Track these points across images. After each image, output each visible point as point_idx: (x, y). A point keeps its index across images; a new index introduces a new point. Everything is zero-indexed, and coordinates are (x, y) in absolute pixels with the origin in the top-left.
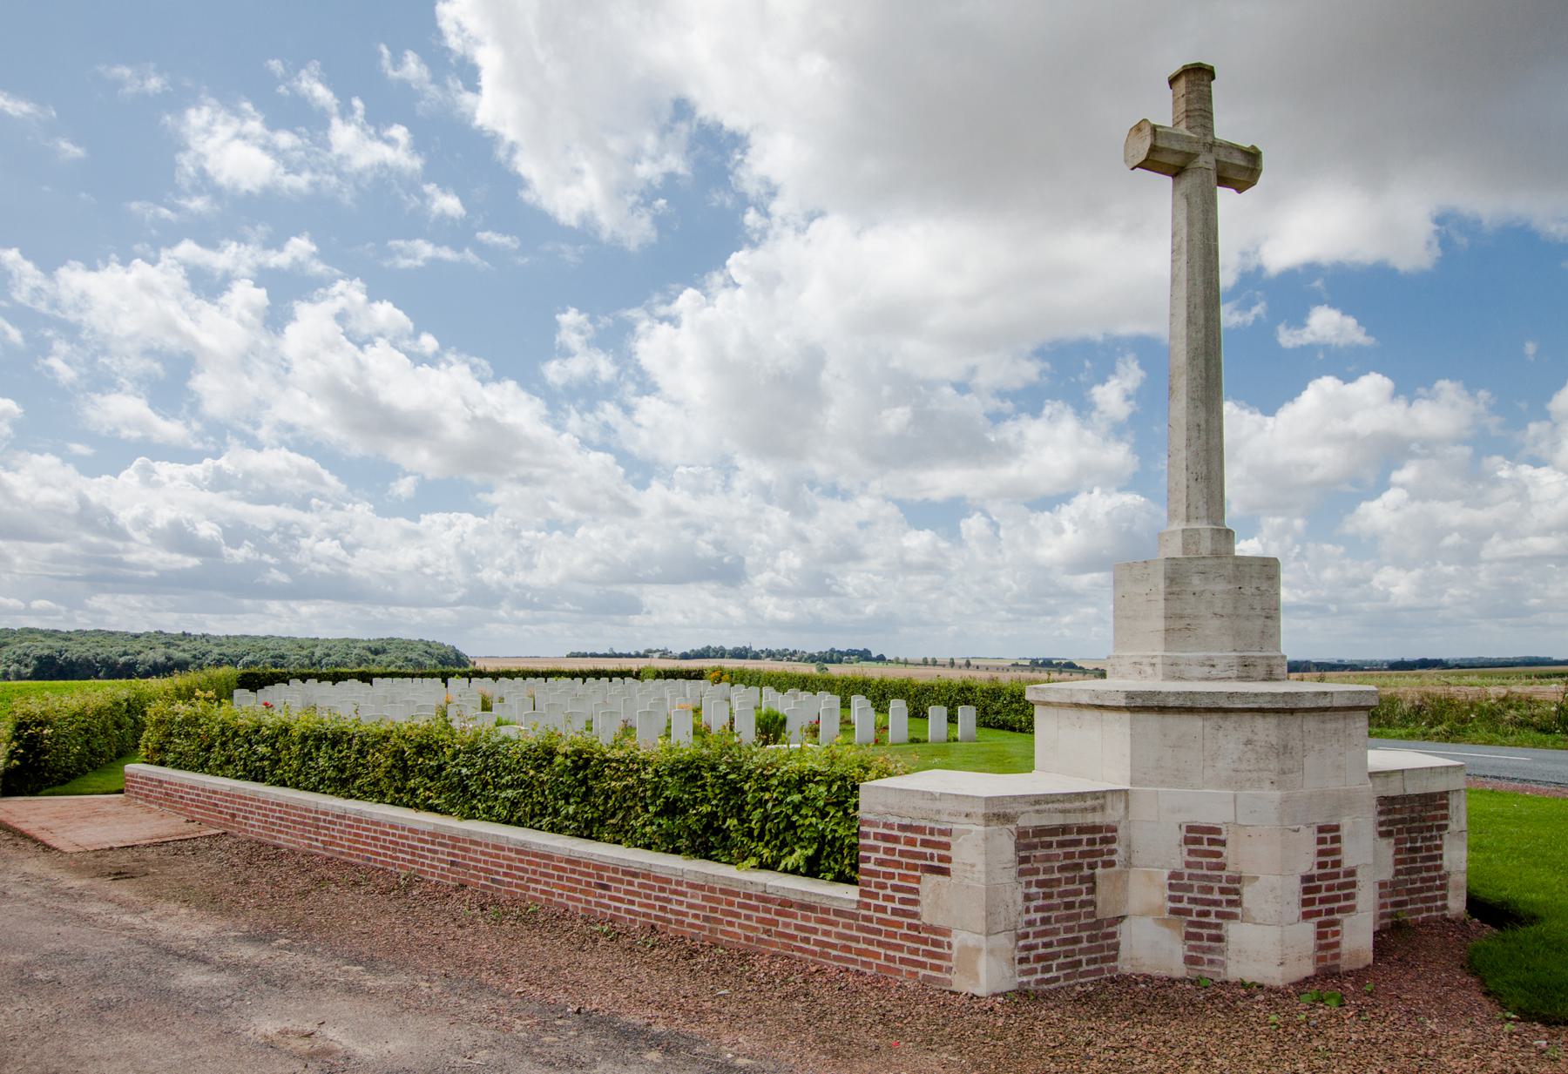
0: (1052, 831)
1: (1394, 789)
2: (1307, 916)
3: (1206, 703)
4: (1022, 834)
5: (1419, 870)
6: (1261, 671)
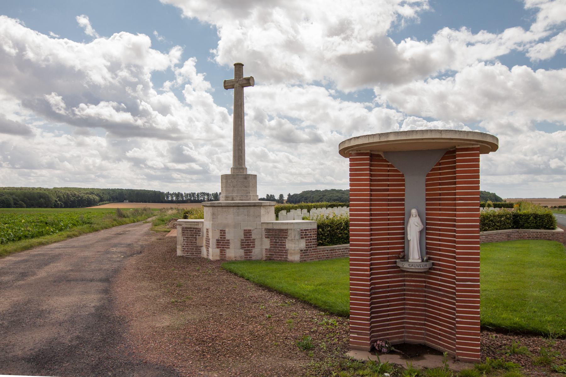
0: (189, 228)
1: (270, 227)
2: (218, 248)
3: (224, 205)
4: (183, 228)
5: (278, 247)
6: (231, 198)
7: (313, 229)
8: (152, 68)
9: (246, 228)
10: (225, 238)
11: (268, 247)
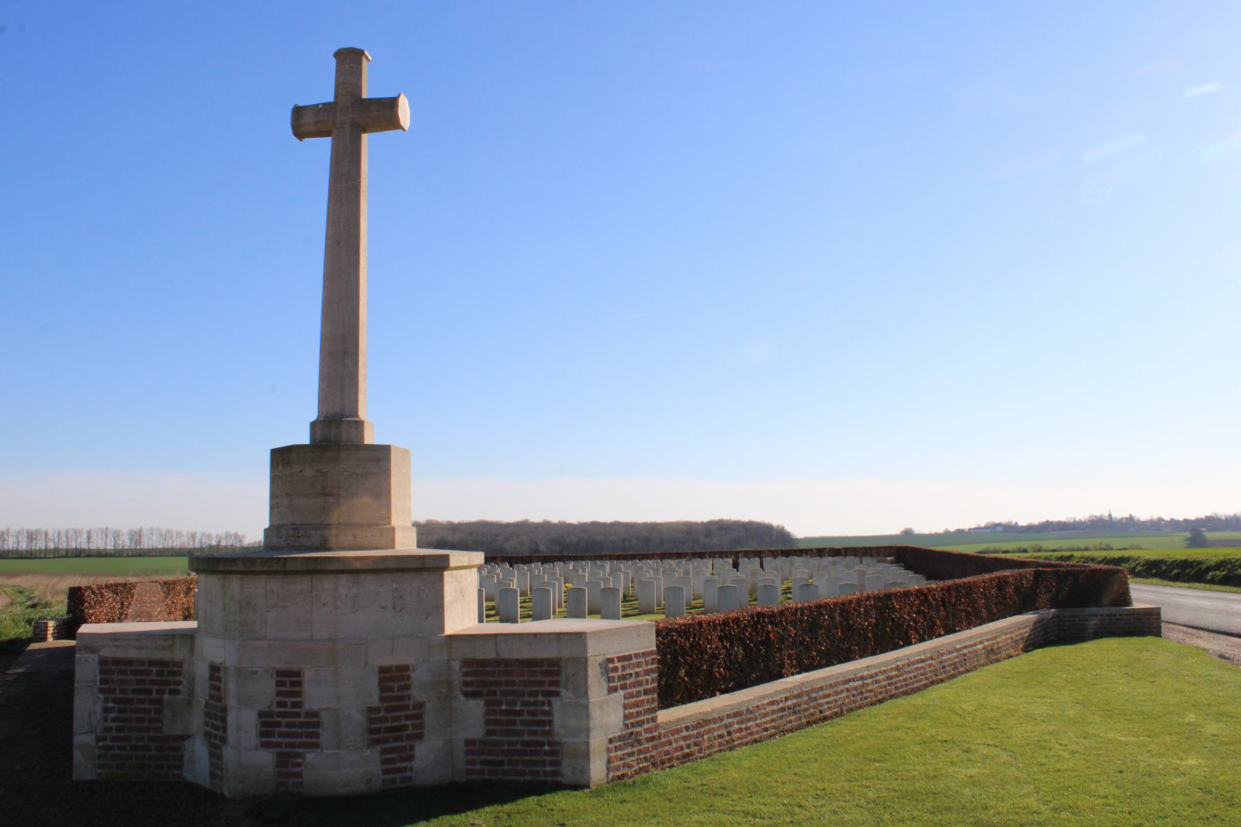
4: (103, 662)
7: (644, 654)
8: (422, 519)
9: (387, 661)
10: (298, 705)
11: (477, 731)
